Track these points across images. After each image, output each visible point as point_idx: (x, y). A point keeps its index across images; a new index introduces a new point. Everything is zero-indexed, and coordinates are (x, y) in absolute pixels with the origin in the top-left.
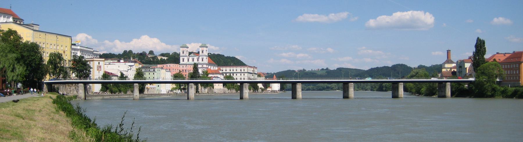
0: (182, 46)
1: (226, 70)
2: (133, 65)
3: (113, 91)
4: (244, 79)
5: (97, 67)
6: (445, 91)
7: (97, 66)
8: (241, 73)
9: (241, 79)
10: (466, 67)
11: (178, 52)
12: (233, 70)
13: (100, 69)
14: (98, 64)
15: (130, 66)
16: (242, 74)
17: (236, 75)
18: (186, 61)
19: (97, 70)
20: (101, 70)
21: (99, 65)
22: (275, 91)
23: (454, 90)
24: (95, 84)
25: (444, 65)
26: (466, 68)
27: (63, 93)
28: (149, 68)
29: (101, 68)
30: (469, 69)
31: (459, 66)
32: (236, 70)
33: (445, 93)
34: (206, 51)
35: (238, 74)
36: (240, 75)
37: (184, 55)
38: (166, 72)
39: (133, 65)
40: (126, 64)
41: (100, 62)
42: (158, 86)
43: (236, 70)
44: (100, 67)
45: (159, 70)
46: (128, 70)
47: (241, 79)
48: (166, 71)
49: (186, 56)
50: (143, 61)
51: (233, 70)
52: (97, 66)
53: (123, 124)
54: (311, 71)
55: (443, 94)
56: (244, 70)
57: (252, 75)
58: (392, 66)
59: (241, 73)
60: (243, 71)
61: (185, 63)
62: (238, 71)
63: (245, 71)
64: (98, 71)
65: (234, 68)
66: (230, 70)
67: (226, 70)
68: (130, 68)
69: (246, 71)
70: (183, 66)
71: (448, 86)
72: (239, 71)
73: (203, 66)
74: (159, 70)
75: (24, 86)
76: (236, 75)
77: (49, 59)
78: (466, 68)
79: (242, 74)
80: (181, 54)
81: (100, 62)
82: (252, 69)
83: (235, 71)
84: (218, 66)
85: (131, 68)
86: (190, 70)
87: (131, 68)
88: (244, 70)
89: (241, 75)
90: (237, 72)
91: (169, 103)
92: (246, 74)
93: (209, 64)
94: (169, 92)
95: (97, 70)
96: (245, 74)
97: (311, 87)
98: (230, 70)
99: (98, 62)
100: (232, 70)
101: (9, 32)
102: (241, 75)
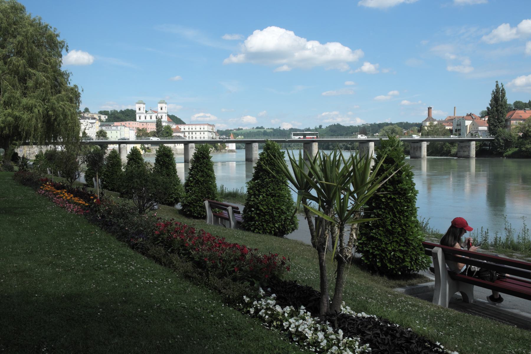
0: (137, 102)
2: (95, 123)
4: (204, 138)
6: (469, 151)
9: (201, 138)
10: (466, 125)
11: (134, 109)
12: (192, 129)
15: (92, 123)
17: (196, 133)
18: (143, 119)
24: (245, 153)
25: (425, 123)
26: (467, 126)
27: (11, 158)
28: (110, 126)
30: (470, 127)
31: (456, 124)
32: (196, 129)
33: (469, 153)
34: (166, 107)
35: (197, 133)
37: (140, 112)
38: (130, 131)
39: (95, 123)
40: (85, 121)
43: (196, 129)
47: (201, 138)
48: (130, 130)
49: (143, 113)
51: (192, 129)
53: (500, 237)
55: (466, 154)
56: (204, 128)
57: (211, 133)
60: (202, 130)
61: (142, 120)
62: (197, 130)
65: (193, 126)
66: (189, 129)
68: (91, 125)
69: (206, 129)
71: (425, 145)
72: (198, 129)
75: (118, 160)
76: (196, 133)
78: (467, 126)
79: (202, 133)
80: (137, 111)
82: (211, 128)
83: (194, 130)
84: (176, 124)
86: (153, 128)
88: (204, 128)
89: (200, 133)
90: (204, 130)
92: (206, 133)
93: (169, 122)
96: (205, 132)
97: (127, 141)
98: (189, 129)
101: (38, 70)
102: (200, 133)
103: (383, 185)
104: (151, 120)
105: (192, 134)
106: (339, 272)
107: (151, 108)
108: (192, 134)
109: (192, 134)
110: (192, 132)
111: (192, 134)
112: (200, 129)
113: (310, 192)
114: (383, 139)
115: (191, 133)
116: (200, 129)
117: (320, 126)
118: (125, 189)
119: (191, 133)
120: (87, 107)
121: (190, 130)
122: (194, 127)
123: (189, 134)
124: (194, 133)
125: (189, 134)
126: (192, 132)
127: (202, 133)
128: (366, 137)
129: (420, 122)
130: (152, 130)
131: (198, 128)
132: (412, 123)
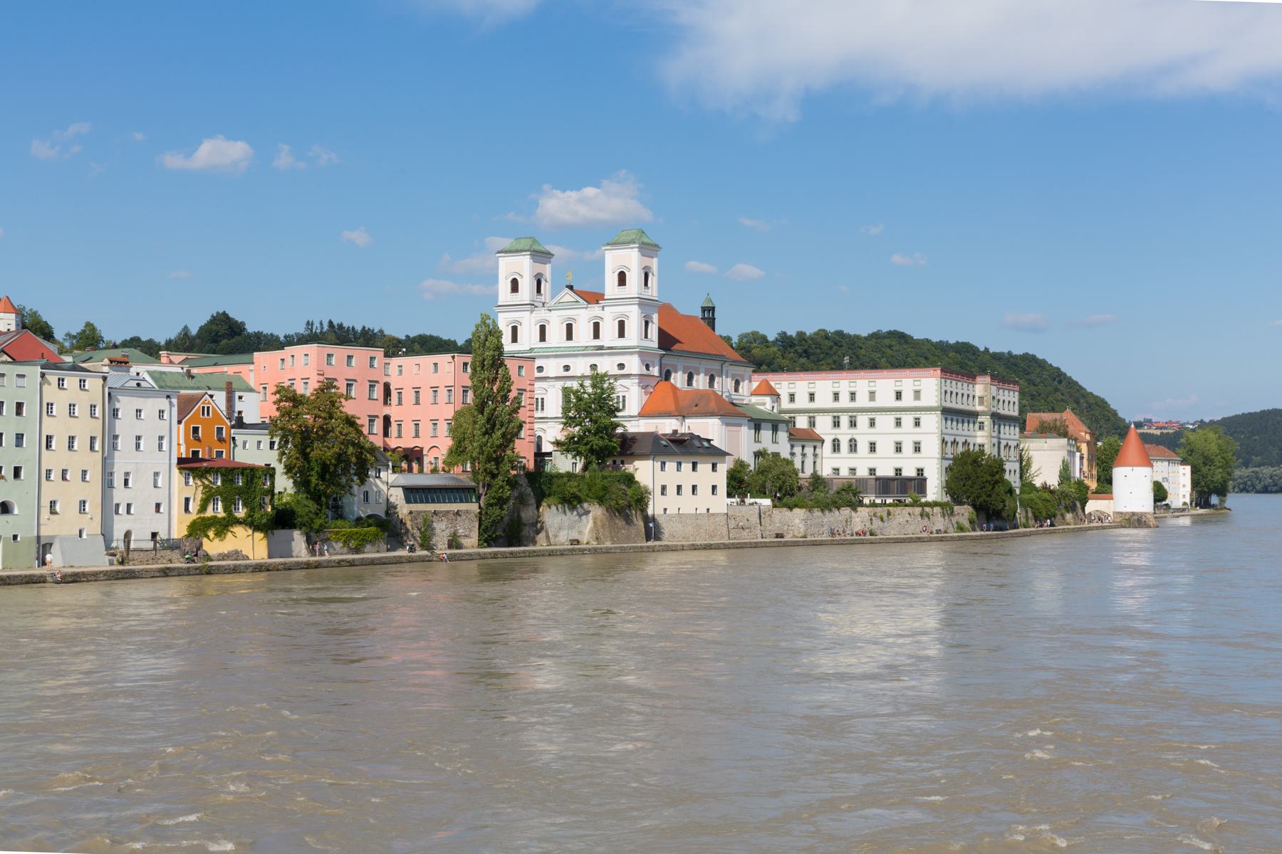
1: (812, 397)
3: (1070, 434)
12: (853, 396)
16: (908, 419)
17: (872, 423)
32: (872, 395)
36: (893, 422)
43: (872, 395)
50: (404, 350)
51: (853, 396)
54: (669, 462)
56: (917, 394)
58: (1261, 411)
60: (908, 401)
62: (878, 403)
66: (836, 396)
67: (812, 397)
70: (436, 364)
72: (885, 398)
73: (567, 368)
76: (872, 423)
77: (53, 337)
83: (862, 401)
88: (917, 394)
89: (898, 423)
90: (872, 404)
91: (137, 628)
94: (1213, 444)
98: (836, 396)
100: (848, 397)
102: (898, 423)
103: (189, 568)
105: (853, 424)
108: (853, 424)
112: (899, 395)
116: (899, 395)
117: (709, 314)
118: (217, 499)
120: (246, 322)
123: (836, 424)
124: (863, 420)
125: (836, 424)
128: (134, 847)
129: (1128, 413)
132: (1258, 410)
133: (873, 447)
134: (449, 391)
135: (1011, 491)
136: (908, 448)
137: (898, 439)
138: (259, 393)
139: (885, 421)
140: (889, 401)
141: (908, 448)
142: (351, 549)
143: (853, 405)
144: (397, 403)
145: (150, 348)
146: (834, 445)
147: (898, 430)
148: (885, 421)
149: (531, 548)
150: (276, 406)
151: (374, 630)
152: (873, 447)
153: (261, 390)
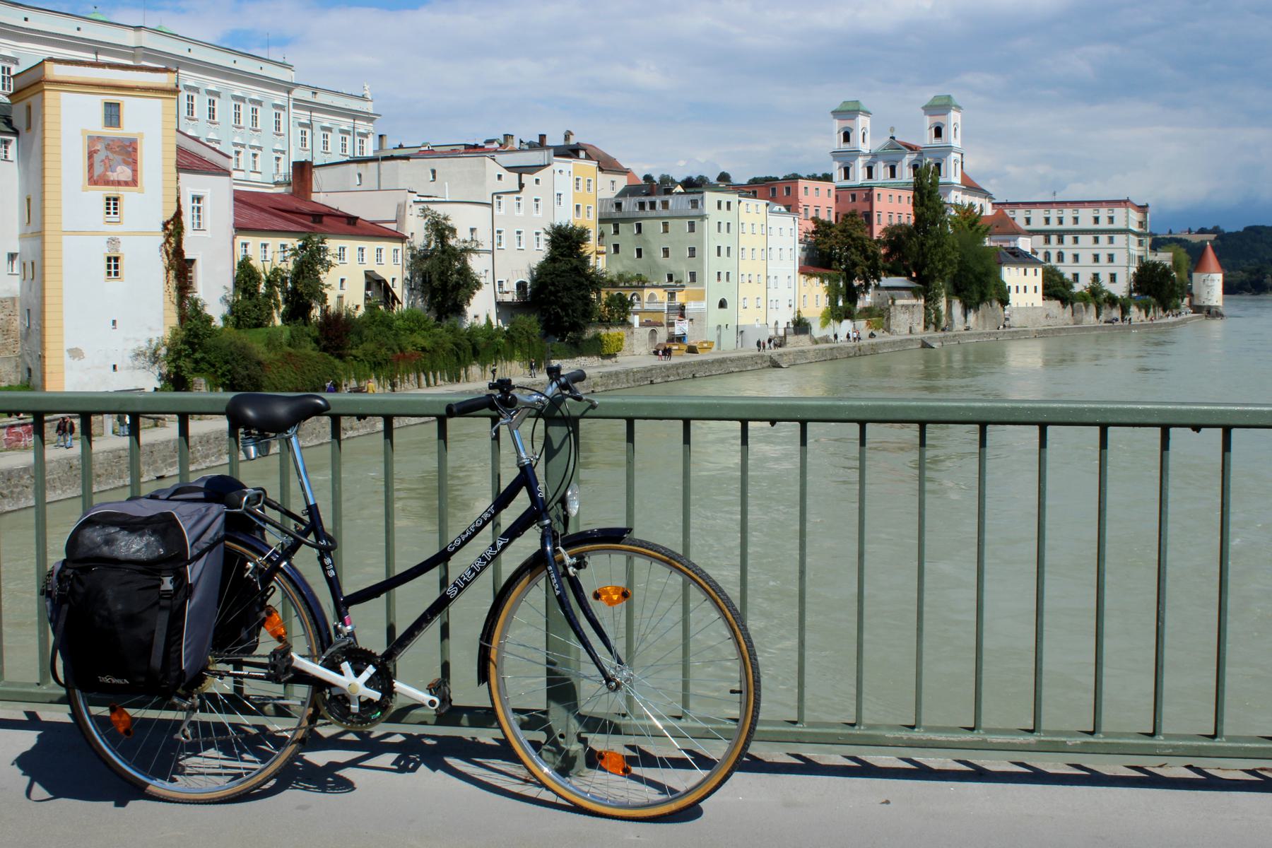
5: (91, 155)
7: (93, 140)
8: (1095, 233)
12: (1061, 221)
13: (123, 172)
14: (96, 124)
15: (520, 170)
19: (93, 181)
20: (134, 182)
21: (112, 132)
22: (1212, 310)
23: (868, 229)
29: (133, 162)
32: (1076, 220)
35: (1081, 237)
41: (131, 106)
42: (537, 181)
43: (1076, 220)
44: (128, 151)
45: (724, 205)
46: (498, 195)
48: (771, 212)
51: (1061, 221)
52: (93, 140)
59: (1095, 233)
60: (1104, 224)
63: (1116, 226)
64: (101, 193)
66: (1047, 221)
68: (511, 180)
74: (724, 205)
81: (131, 106)
83: (1069, 224)
85: (521, 186)
87: (521, 186)
89: (1096, 240)
95: (93, 181)
98: (1047, 221)
99: (661, 222)
100: (1106, 220)
102: (1096, 240)
104: (870, 181)
106: (153, 419)
107: (892, 129)
109: (1061, 241)
110: (1061, 235)
111: (1061, 241)
113: (46, 93)
114: (128, 422)
115: (1054, 238)
116: (1096, 220)
119: (1054, 238)
120: (705, 175)
121: (1054, 225)
122: (1068, 214)
126: (1061, 235)
127: (1103, 238)
130: (895, 221)
131: (1086, 218)
133: (1076, 257)
134: (829, 211)
135: (844, 279)
136: (1103, 258)
137: (1096, 252)
138: (29, 108)
139: (1086, 240)
140: (1090, 225)
141: (1103, 258)
142: (585, 150)
143: (1060, 227)
144: (722, 224)
145: (981, 774)
146: (1059, 257)
147: (1076, 246)
148: (1068, 239)
149: (240, 672)
150: (932, 327)
151: (29, 370)
152: (1076, 257)
153: (233, 155)
